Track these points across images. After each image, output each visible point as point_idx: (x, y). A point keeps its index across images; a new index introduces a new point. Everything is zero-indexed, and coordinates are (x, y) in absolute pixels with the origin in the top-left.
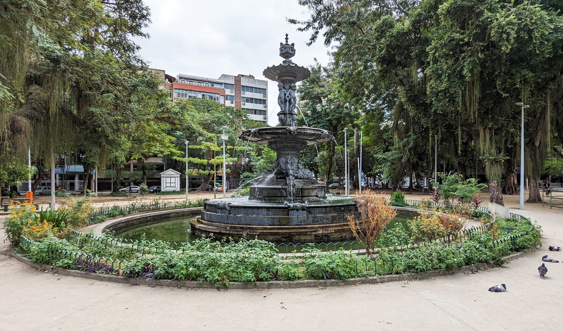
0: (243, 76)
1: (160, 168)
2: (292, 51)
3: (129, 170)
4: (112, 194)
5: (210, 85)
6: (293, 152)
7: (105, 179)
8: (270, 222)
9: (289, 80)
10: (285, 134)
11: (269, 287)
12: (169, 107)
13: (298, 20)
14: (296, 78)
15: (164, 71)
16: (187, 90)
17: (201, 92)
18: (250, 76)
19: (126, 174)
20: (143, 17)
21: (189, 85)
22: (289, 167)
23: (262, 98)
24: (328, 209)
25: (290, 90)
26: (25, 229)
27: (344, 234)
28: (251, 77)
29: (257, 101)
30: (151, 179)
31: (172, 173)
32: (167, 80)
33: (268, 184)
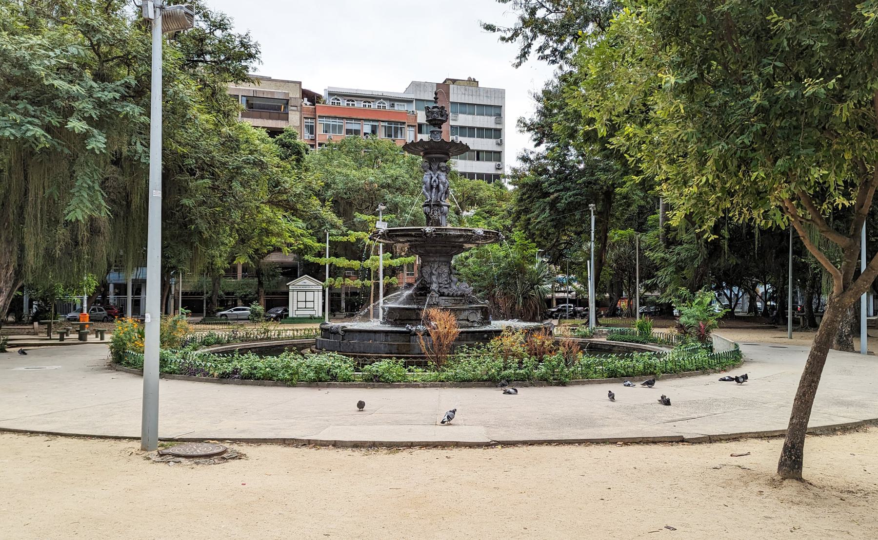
0: (454, 81)
1: (291, 272)
2: (442, 116)
3: (235, 277)
4: (204, 320)
6: (442, 259)
7: (192, 294)
8: (386, 350)
9: (436, 158)
10: (420, 236)
11: (328, 386)
12: (287, 186)
13: (497, 25)
14: (448, 155)
15: (300, 83)
17: (369, 120)
18: (470, 80)
19: (230, 284)
20: (251, 56)
22: (434, 280)
23: (493, 126)
25: (439, 172)
26: (129, 345)
28: (473, 82)
29: (483, 132)
30: (273, 294)
31: (308, 282)
32: (306, 99)
33: (404, 303)
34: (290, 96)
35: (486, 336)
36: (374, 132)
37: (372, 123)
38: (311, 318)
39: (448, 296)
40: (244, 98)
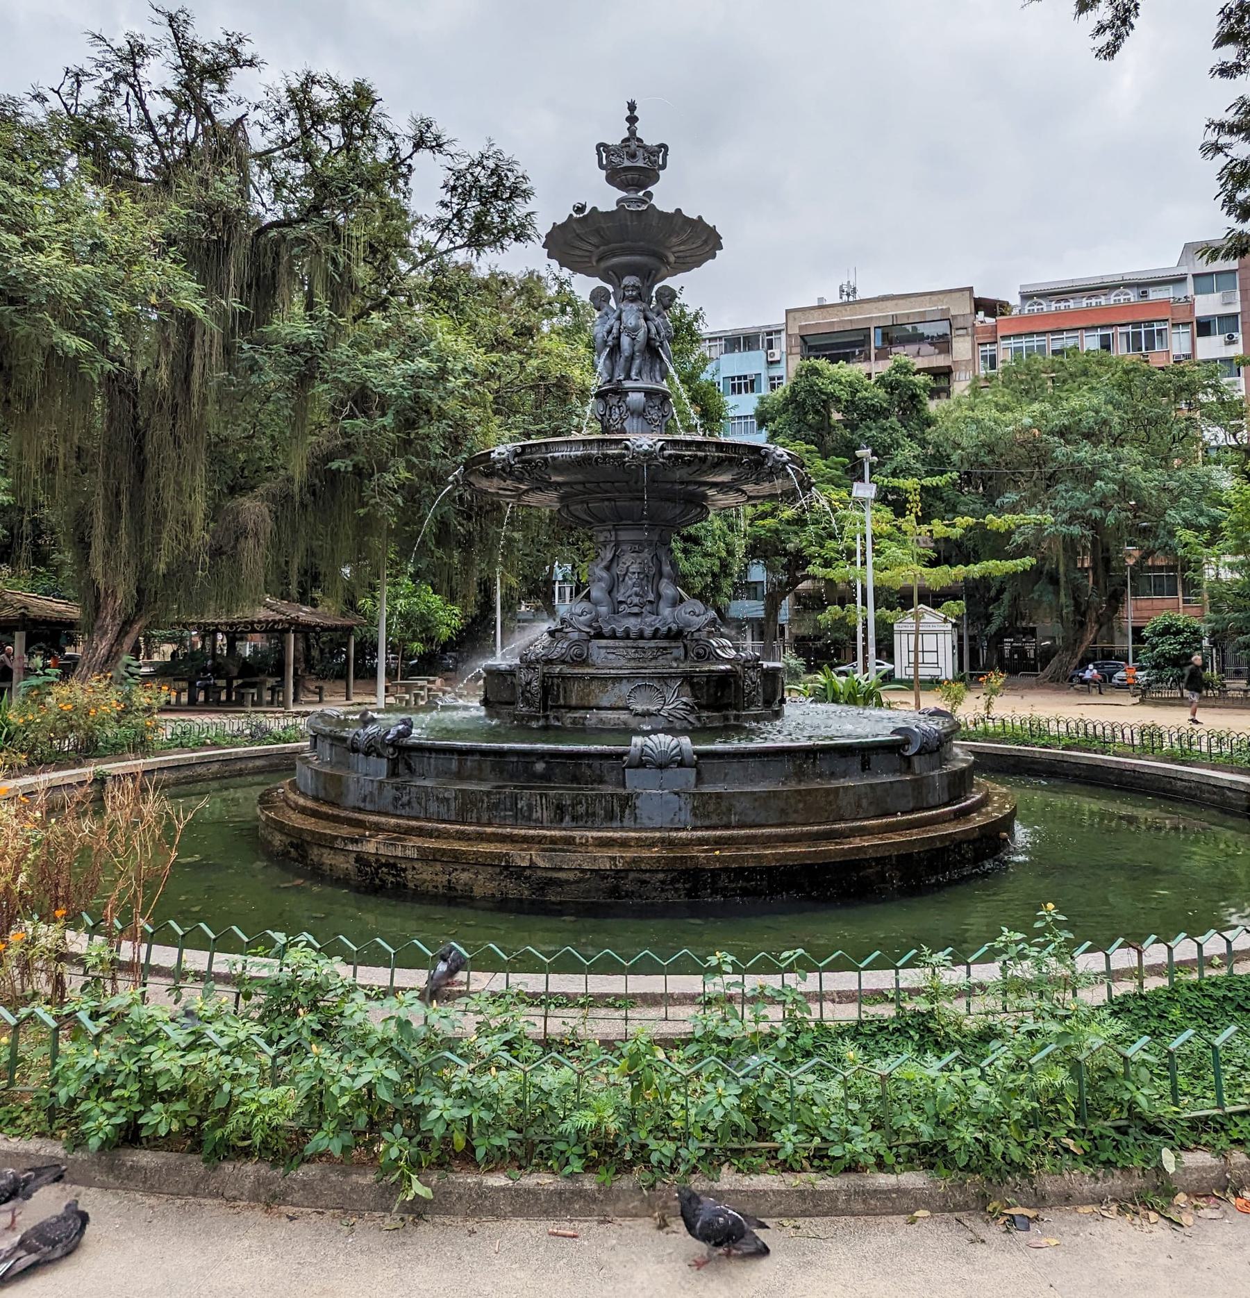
5: (1133, 296)
15: (971, 289)
16: (1044, 333)
17: (1095, 328)
20: (515, 192)
21: (1058, 315)
24: (470, 762)
27: (465, 876)
32: (981, 314)
34: (953, 312)
35: (540, 767)
36: (1106, 345)
37: (1100, 332)
38: (931, 682)
39: (613, 636)
40: (879, 331)
